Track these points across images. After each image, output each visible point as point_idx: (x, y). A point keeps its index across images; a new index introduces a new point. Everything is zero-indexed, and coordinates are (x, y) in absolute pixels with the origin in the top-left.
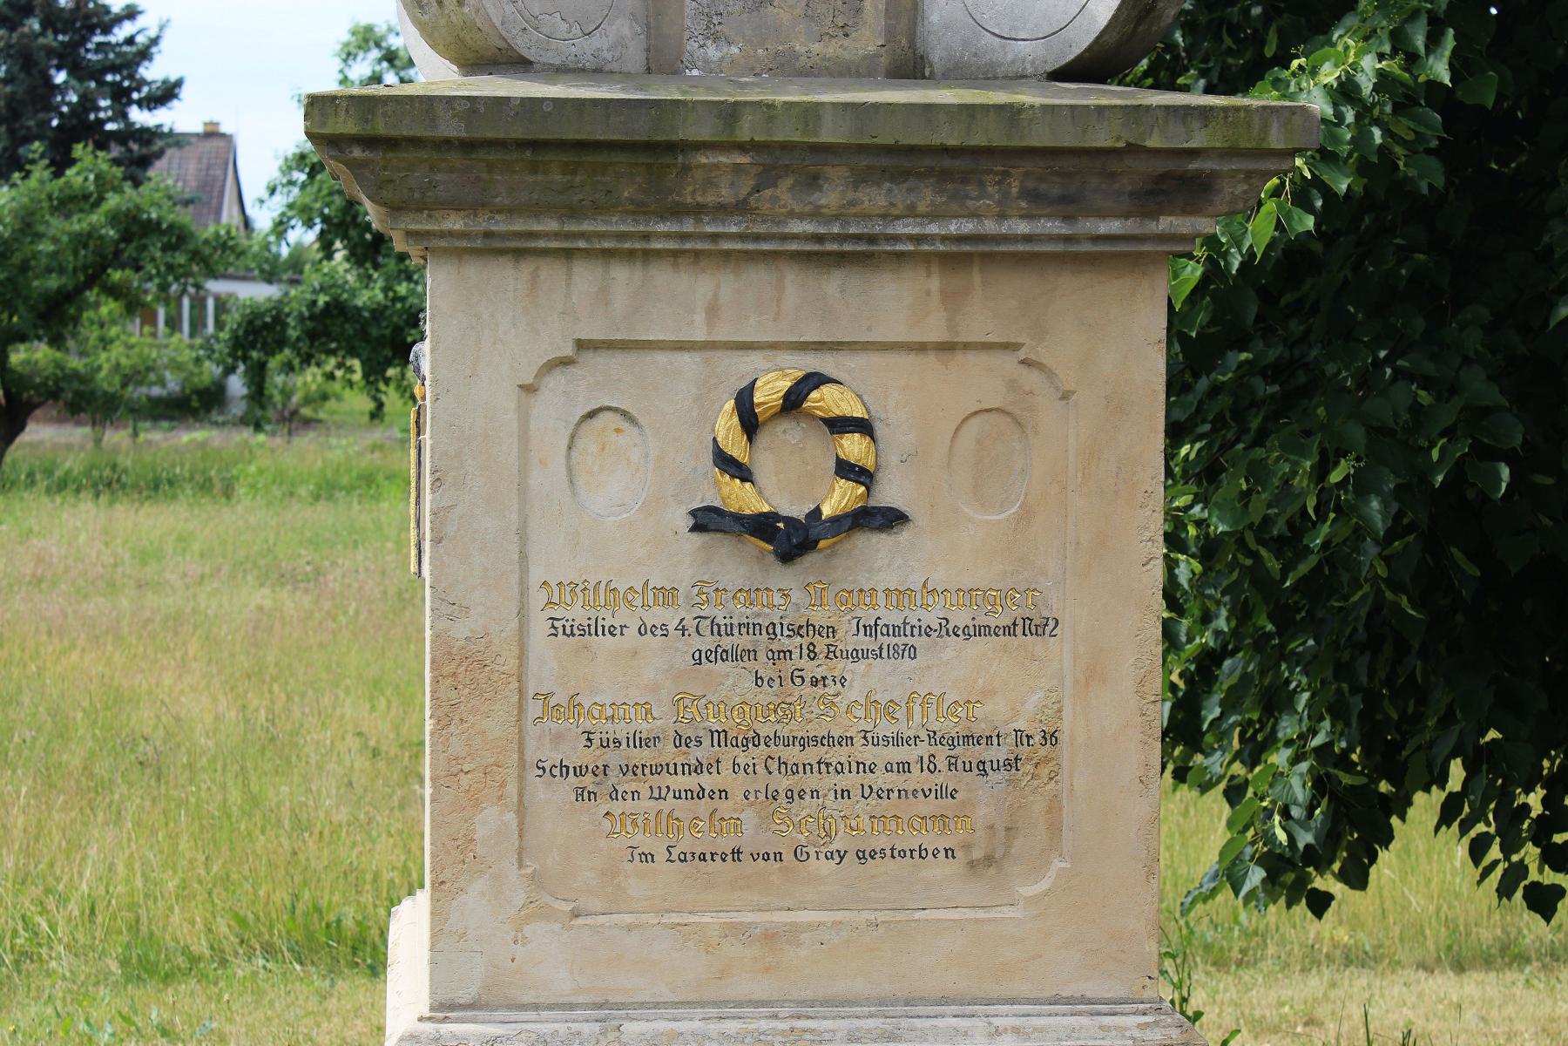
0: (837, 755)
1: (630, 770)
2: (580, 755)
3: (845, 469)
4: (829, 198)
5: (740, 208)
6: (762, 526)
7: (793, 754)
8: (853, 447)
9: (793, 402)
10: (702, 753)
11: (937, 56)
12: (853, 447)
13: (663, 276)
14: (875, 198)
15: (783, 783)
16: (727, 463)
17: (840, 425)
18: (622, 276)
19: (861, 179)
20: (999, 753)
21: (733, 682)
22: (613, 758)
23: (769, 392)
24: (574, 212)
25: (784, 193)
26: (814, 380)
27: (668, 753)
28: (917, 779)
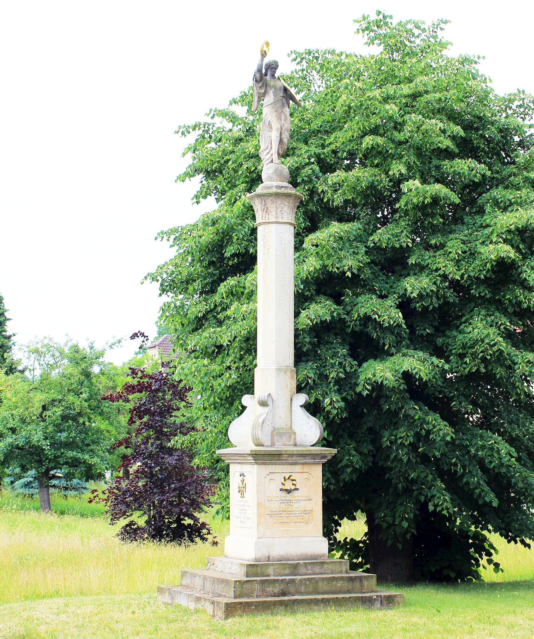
0: (293, 513)
1: (275, 514)
2: (270, 513)
3: (293, 484)
4: (294, 458)
5: (286, 460)
6: (286, 490)
7: (289, 513)
8: (294, 482)
9: (289, 478)
10: (281, 513)
11: (298, 444)
12: (294, 482)
13: (277, 466)
14: (298, 458)
15: (288, 515)
16: (283, 484)
17: (293, 480)
18: (274, 466)
19: (297, 457)
20: (307, 512)
21: (284, 505)
22: (273, 513)
23: (287, 477)
24: (271, 460)
25: (290, 458)
26: (291, 476)
27: (278, 513)
28: (300, 515)
